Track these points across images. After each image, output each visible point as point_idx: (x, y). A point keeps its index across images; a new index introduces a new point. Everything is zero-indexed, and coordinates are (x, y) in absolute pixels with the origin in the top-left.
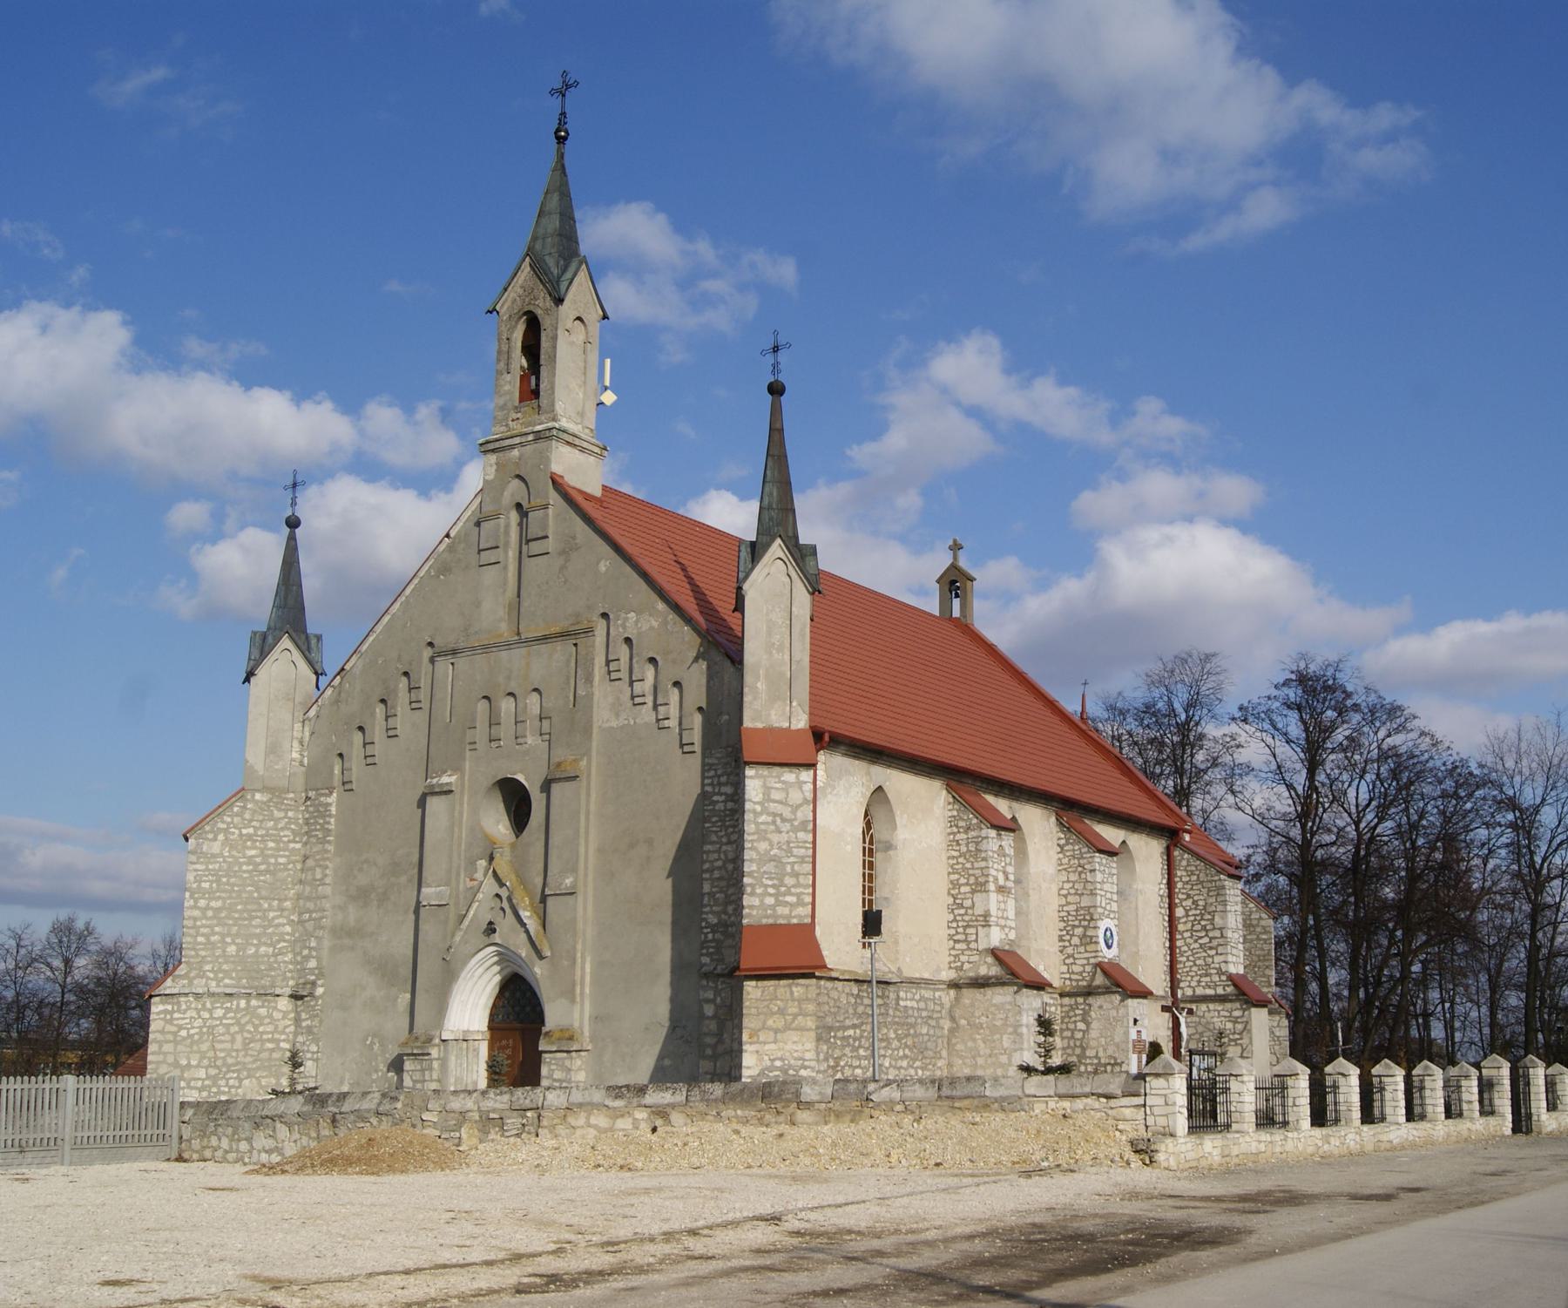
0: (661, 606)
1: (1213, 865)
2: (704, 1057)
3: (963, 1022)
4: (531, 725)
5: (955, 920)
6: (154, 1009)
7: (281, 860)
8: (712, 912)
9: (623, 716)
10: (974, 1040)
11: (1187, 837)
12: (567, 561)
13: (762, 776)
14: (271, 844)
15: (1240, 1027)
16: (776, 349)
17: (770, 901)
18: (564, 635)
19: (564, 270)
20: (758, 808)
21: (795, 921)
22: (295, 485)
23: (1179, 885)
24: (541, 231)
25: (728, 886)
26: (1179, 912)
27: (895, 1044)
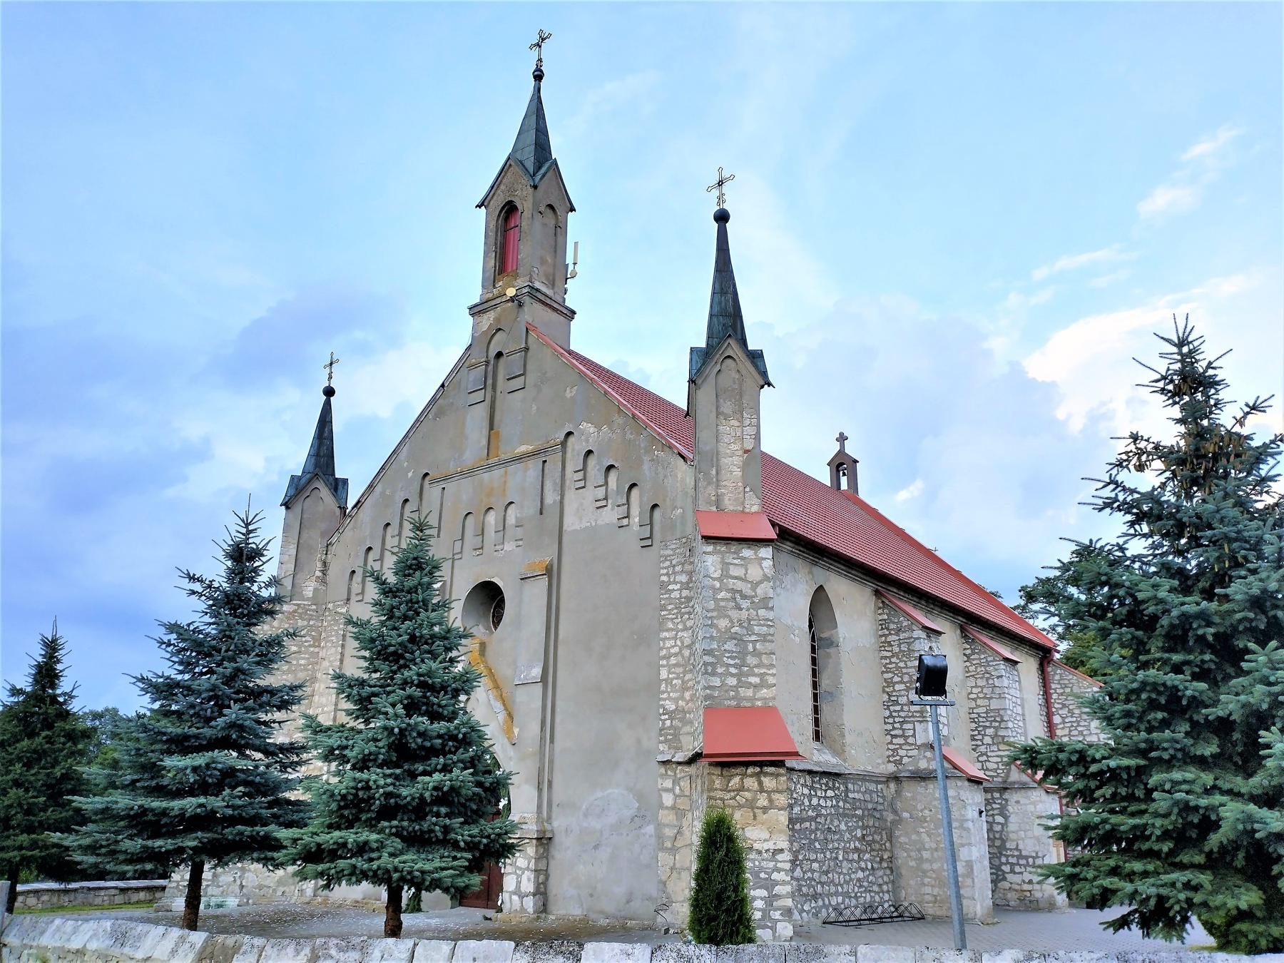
2: (663, 849)
3: (906, 815)
5: (891, 716)
7: (302, 662)
8: (669, 698)
10: (918, 833)
13: (719, 552)
16: (720, 183)
17: (732, 681)
21: (759, 703)
23: (1055, 696)
24: (520, 146)
25: (685, 673)
26: (1057, 719)
27: (847, 836)
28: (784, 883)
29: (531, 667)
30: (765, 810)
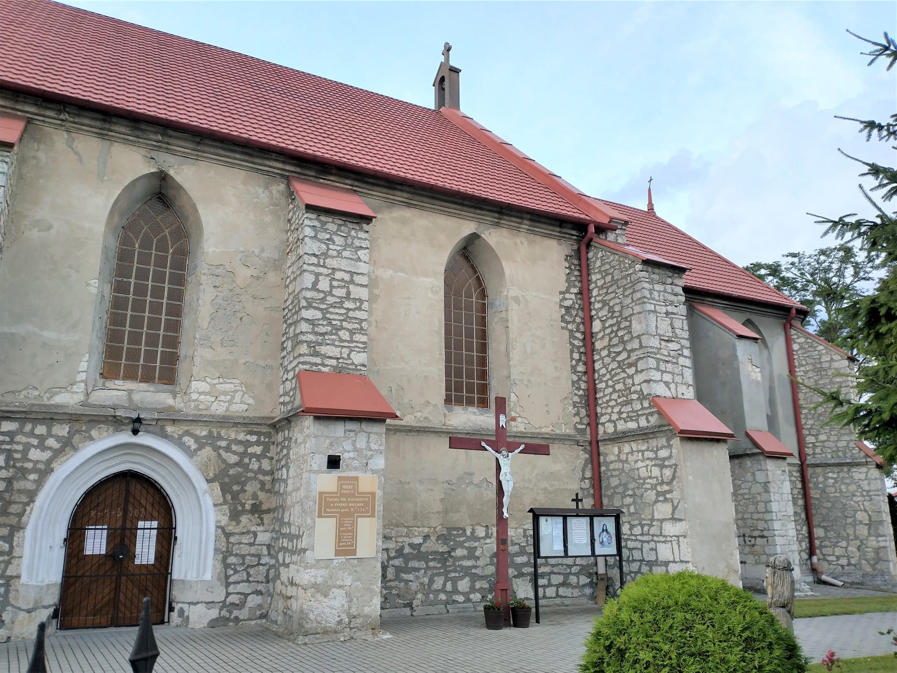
15: (668, 473)
23: (595, 293)
26: (597, 326)
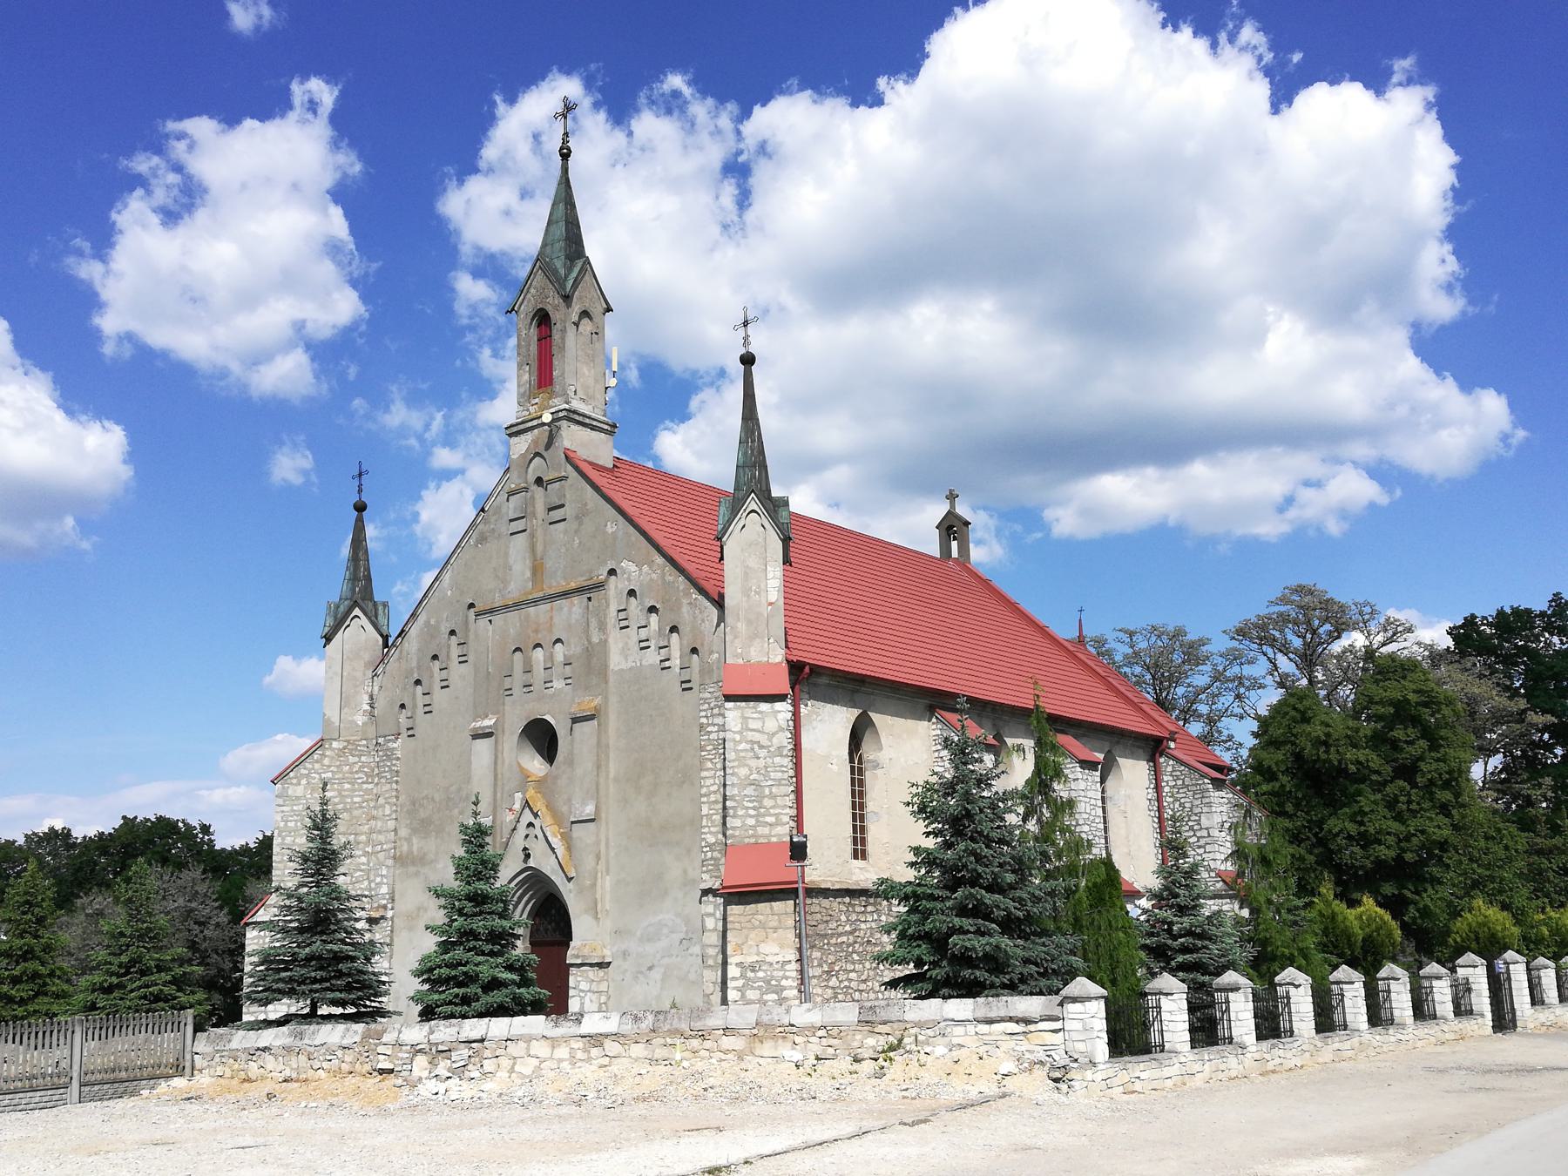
0: (660, 560)
1: (1196, 770)
4: (558, 669)
6: (248, 935)
9: (631, 659)
11: (1172, 745)
12: (581, 524)
14: (347, 786)
17: (751, 822)
18: (579, 591)
19: (569, 270)
20: (738, 737)
21: (774, 840)
22: (360, 475)
23: (1167, 789)
24: (550, 238)
28: (791, 988)
29: (584, 804)
30: (775, 929)
